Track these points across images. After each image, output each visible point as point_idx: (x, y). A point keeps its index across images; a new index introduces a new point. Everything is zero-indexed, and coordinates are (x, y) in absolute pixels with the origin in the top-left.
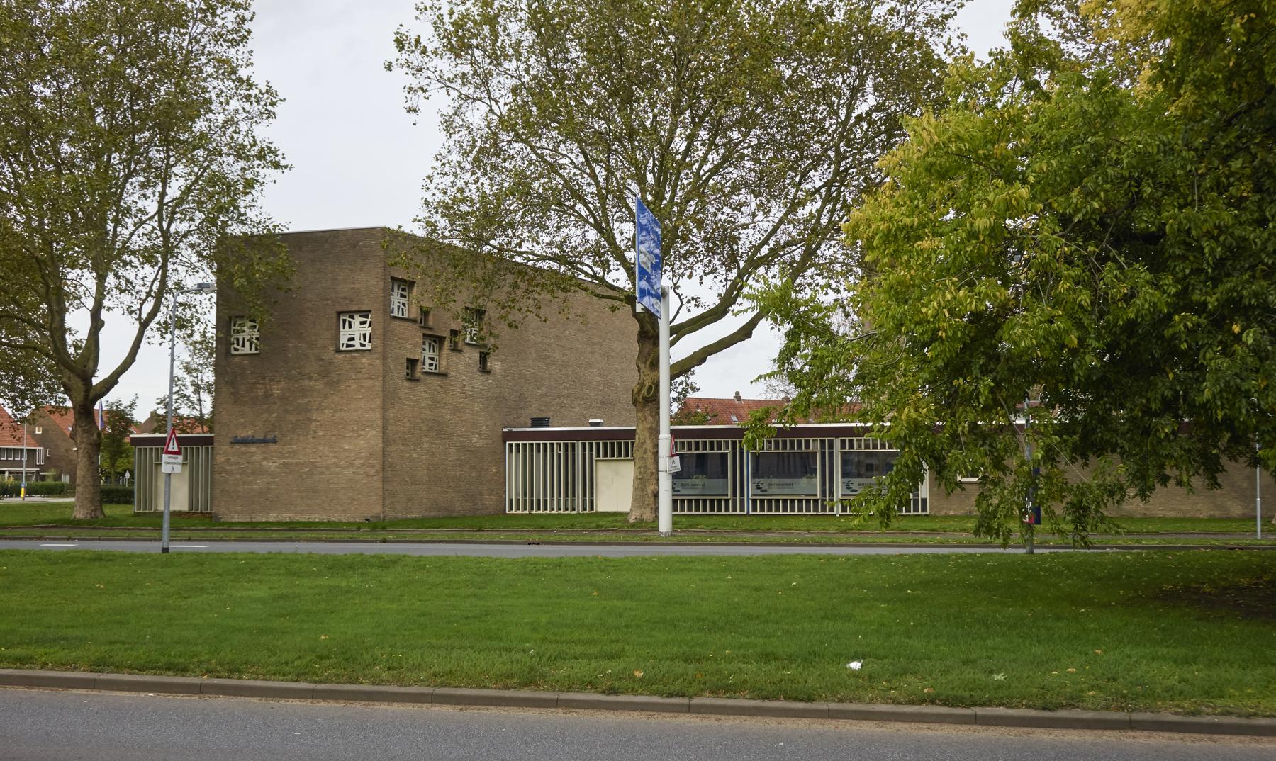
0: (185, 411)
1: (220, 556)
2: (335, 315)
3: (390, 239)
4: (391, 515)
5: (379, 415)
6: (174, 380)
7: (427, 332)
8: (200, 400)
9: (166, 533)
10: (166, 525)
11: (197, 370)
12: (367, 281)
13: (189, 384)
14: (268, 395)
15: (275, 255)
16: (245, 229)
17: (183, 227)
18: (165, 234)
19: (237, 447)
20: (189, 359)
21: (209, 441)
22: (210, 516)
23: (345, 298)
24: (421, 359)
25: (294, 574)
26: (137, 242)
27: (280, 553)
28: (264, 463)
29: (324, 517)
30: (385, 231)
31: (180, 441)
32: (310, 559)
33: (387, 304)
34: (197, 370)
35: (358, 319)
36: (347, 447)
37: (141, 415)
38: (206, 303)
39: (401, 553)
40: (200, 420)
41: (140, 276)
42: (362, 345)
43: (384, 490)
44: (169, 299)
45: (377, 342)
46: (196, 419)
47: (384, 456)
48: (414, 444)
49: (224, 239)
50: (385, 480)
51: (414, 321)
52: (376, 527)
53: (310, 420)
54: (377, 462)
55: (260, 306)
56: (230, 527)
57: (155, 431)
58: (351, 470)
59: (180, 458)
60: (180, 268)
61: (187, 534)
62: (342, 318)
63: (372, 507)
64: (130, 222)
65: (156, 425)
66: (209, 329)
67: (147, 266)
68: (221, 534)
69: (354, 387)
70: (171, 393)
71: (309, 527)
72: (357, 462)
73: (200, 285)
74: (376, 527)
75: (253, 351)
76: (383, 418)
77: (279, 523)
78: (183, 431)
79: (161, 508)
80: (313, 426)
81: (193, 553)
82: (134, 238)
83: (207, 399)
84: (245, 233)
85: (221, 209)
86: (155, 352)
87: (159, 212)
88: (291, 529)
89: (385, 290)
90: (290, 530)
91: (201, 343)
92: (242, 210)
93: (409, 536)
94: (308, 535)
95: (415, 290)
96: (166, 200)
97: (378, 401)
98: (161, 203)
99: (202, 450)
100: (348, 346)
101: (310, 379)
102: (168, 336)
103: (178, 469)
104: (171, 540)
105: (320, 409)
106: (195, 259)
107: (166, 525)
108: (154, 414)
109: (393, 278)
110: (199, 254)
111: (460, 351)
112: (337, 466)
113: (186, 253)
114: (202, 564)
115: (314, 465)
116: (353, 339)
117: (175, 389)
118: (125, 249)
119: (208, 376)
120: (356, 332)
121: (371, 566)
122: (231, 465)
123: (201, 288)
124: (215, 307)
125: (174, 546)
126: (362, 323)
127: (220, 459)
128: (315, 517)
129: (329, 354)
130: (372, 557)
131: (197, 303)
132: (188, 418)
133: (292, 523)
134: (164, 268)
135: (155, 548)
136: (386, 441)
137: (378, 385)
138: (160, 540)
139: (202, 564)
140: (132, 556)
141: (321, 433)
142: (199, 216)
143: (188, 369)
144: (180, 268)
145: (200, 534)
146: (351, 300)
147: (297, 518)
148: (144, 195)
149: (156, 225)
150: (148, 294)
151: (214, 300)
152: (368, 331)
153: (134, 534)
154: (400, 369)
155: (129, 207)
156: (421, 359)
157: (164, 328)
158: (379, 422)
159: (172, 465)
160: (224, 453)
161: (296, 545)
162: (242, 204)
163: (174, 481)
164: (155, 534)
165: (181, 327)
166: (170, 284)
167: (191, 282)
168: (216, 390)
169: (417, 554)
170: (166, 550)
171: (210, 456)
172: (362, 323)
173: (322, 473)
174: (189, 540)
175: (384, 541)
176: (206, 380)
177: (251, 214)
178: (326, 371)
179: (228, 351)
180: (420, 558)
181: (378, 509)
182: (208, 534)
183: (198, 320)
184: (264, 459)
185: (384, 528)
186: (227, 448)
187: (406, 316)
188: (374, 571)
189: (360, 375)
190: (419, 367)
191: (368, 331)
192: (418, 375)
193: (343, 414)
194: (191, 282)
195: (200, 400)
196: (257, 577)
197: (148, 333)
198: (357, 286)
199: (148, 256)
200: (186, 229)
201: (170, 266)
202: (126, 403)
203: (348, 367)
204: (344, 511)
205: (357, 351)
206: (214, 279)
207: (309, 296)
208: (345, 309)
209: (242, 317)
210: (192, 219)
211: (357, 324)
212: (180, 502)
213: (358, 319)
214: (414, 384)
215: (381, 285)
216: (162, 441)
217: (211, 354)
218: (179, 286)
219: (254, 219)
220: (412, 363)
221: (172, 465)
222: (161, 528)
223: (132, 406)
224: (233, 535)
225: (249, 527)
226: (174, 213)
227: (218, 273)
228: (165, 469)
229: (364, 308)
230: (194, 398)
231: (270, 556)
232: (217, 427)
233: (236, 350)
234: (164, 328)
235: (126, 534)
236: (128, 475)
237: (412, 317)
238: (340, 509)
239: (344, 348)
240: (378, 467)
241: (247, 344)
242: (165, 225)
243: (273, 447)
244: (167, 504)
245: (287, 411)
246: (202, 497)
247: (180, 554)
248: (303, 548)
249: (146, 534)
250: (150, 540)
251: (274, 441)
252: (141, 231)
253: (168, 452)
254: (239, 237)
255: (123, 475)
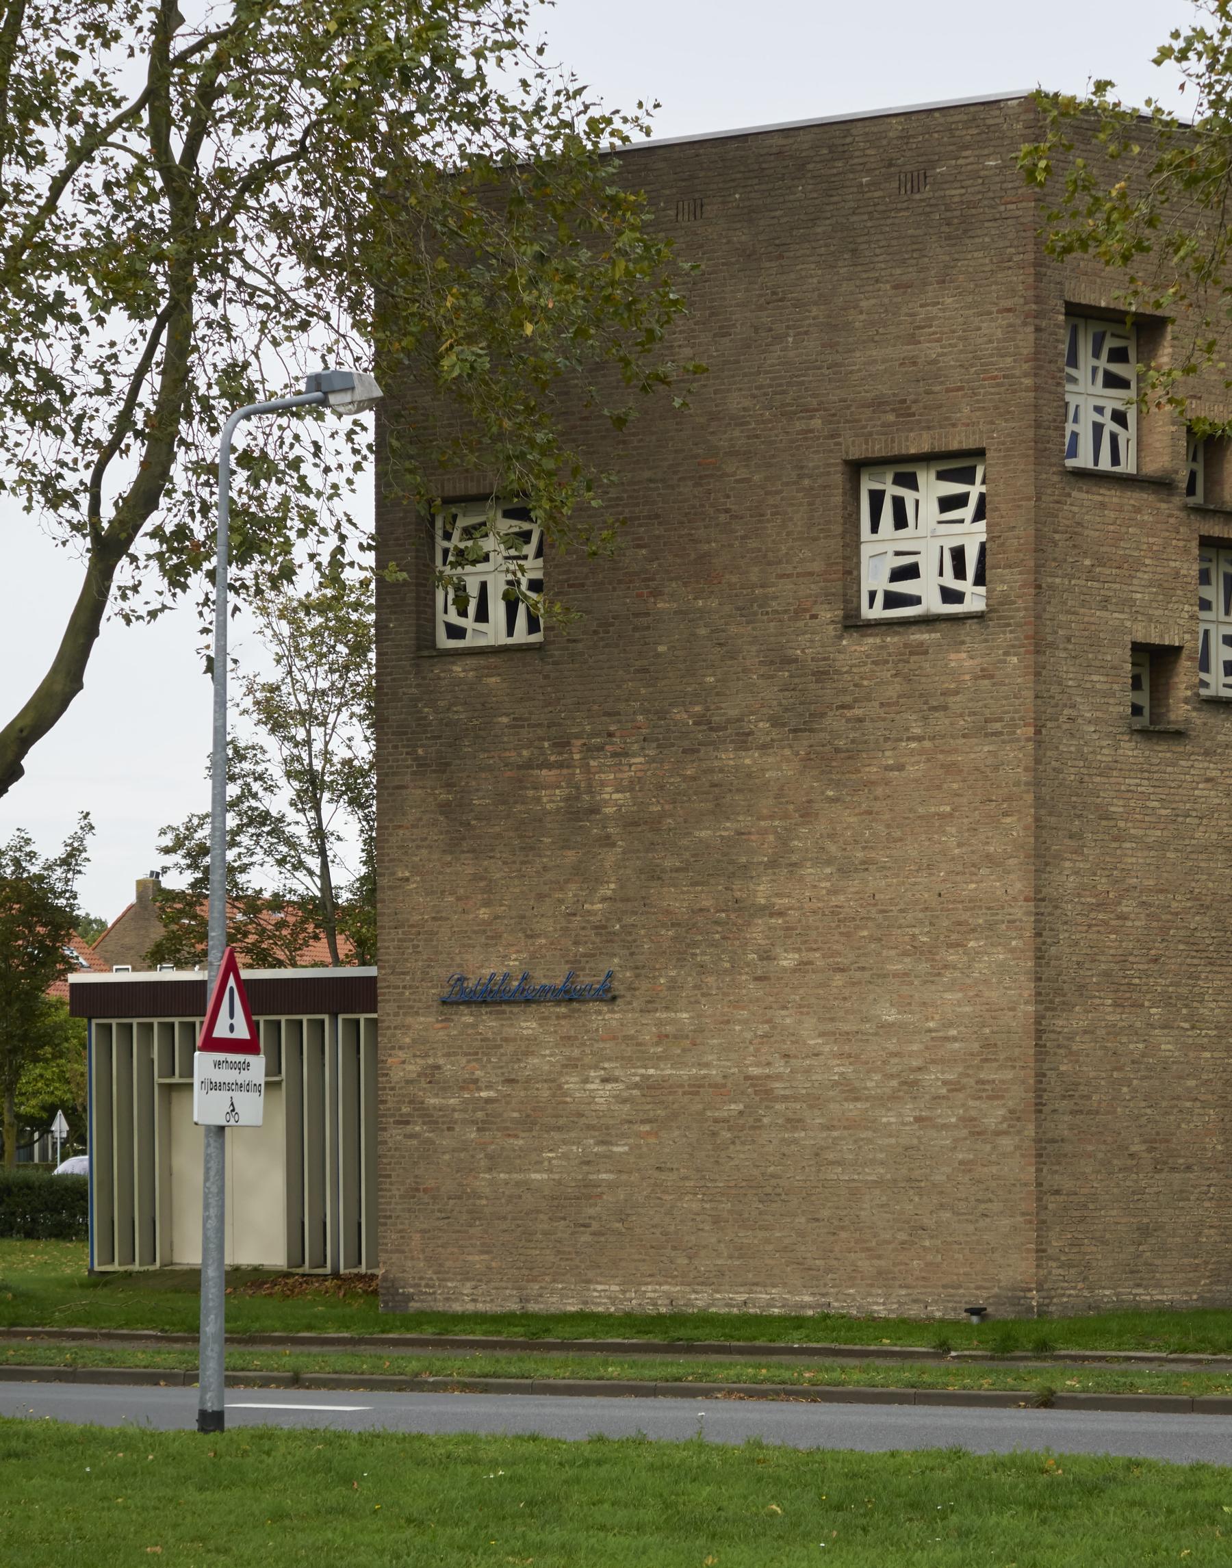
0: (264, 878)
1: (410, 1450)
2: (838, 478)
3: (1064, 134)
4: (1071, 1294)
5: (1019, 885)
6: (227, 759)
7: (1217, 529)
8: (319, 834)
9: (211, 1352)
10: (212, 1326)
11: (307, 717)
12: (960, 328)
13: (276, 771)
14: (580, 812)
15: (598, 240)
16: (489, 142)
17: (239, 148)
18: (180, 181)
19: (466, 1017)
20: (273, 674)
21: (355, 996)
22: (365, 1288)
23: (878, 404)
24: (1193, 645)
25: (696, 1526)
26: (81, 219)
27: (640, 1441)
28: (571, 1082)
29: (805, 1300)
30: (1040, 106)
31: (258, 998)
32: (753, 1465)
33: (1050, 419)
34: (307, 717)
35: (931, 488)
36: (890, 1016)
37: (102, 895)
38: (338, 451)
39: (1119, 1454)
40: (321, 912)
41: (92, 352)
42: (950, 596)
43: (1042, 1191)
44: (199, 440)
45: (1007, 580)
46: (305, 903)
47: (1041, 1051)
48: (1166, 1000)
49: (405, 181)
50: (1045, 1151)
51: (1160, 485)
52: (1011, 1342)
53: (746, 910)
54: (1013, 1080)
55: (545, 451)
56: (445, 1331)
57: (157, 957)
58: (909, 1111)
59: (258, 1063)
60: (236, 313)
61: (288, 1358)
62: (867, 485)
63: (1005, 1268)
64: (51, 137)
65: (158, 932)
66: (351, 549)
67: (118, 316)
68: (413, 1362)
69: (915, 769)
70: (222, 805)
71: (749, 1336)
72: (932, 1077)
73: (316, 382)
74: (1011, 1342)
75: (521, 635)
76: (1038, 898)
77: (631, 1321)
78: (262, 958)
79: (190, 1254)
80: (757, 933)
81: (312, 1436)
82: (68, 203)
83: (346, 828)
84: (479, 161)
85: (387, 69)
86: (156, 651)
87: (155, 95)
88: (677, 1344)
89: (1038, 358)
90: (670, 1348)
91: (323, 607)
92: (467, 67)
93: (1146, 1383)
94: (745, 1369)
95: (1165, 356)
96: (179, 45)
97: (1017, 826)
98: (159, 52)
99: (335, 1030)
100: (893, 600)
101: (743, 741)
102: (198, 583)
103: (251, 1108)
104: (231, 1382)
105: (782, 861)
106: (292, 275)
107: (212, 1326)
108: (151, 892)
109: (1078, 313)
110: (308, 253)
111: (1179, 735)
112: (854, 1094)
113: (259, 251)
114: (347, 1479)
115: (762, 1090)
116: (911, 572)
117: (233, 790)
118: (35, 252)
119: (350, 739)
120: (925, 540)
121: (1002, 1503)
122: (444, 1088)
123: (320, 394)
124: (370, 467)
125: (247, 1406)
126: (948, 504)
127: (402, 1066)
128: (772, 1299)
129: (817, 636)
130: (1000, 1465)
131: (303, 451)
132: (277, 902)
133: (746, 1321)
134: (177, 319)
135: (172, 1409)
136: (1049, 995)
137: (1015, 758)
138: (189, 1378)
139: (347, 1479)
140: (91, 1439)
141: (788, 960)
142: (305, 100)
143: (274, 715)
144: (236, 313)
145: (337, 1359)
146: (903, 410)
147: (699, 1300)
148: (98, 29)
149: (143, 145)
150: (124, 422)
151: (366, 438)
152: (972, 535)
153: (93, 1355)
154: (1108, 689)
155: (50, 80)
156: (1193, 645)
157: (181, 555)
158: (1021, 912)
159: (227, 1094)
160: (417, 1042)
161: (699, 1411)
162: (467, 41)
163: (236, 1154)
164: (168, 1358)
165: (244, 551)
166: (203, 378)
167: (280, 368)
168: (383, 791)
169: (1183, 1458)
170: (211, 1421)
171: (365, 1050)
172: (948, 504)
173: (794, 1123)
174: (295, 1381)
175: (1048, 1401)
176: (341, 753)
177: (503, 80)
178: (806, 709)
179: (425, 639)
180: (1195, 1476)
181: (1017, 1269)
182: (364, 1362)
183: (309, 518)
184: (571, 1064)
185: (1043, 1348)
186: (424, 1022)
187: (1128, 466)
188: (1009, 1523)
189: (941, 722)
190: (1184, 678)
191: (972, 535)
192: (1180, 710)
193: (875, 881)
194: (280, 368)
195: (319, 834)
196: (555, 1536)
197: (123, 573)
198: (930, 350)
199: (119, 275)
200: (254, 156)
201: (200, 310)
202: (49, 849)
203: (893, 691)
204: (884, 1278)
205: (928, 621)
206: (364, 349)
207: (736, 402)
208: (878, 449)
209: (479, 499)
210: (282, 117)
211: (930, 509)
212: (260, 1240)
213: (931, 488)
214: (1163, 752)
215: (1026, 340)
216: (190, 998)
217: (358, 650)
218: (236, 385)
219: (515, 97)
220: (1154, 662)
221: (227, 1094)
222: (192, 1334)
223: (71, 859)
224: (458, 1364)
225: (517, 1333)
226: (209, 93)
227: (385, 325)
228: (205, 1107)
229: (958, 441)
230: (299, 827)
231: (602, 1452)
232: (388, 942)
233: (456, 632)
234: (181, 555)
235: (66, 1353)
236: (60, 1126)
237: (1155, 465)
238: (865, 1264)
239: (877, 612)
240: (1018, 1096)
241: (497, 610)
242: (177, 143)
243: (602, 1018)
244: (216, 1238)
245: (654, 874)
246: (336, 1212)
247: (264, 1437)
248: (728, 1421)
249: (139, 1357)
250: (151, 1379)
251: (606, 995)
252: (94, 175)
253: (213, 1044)
254: (458, 174)
255: (45, 1126)
